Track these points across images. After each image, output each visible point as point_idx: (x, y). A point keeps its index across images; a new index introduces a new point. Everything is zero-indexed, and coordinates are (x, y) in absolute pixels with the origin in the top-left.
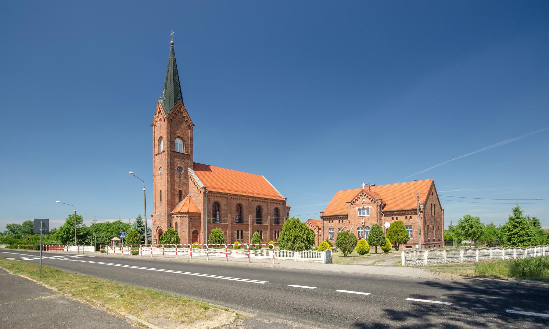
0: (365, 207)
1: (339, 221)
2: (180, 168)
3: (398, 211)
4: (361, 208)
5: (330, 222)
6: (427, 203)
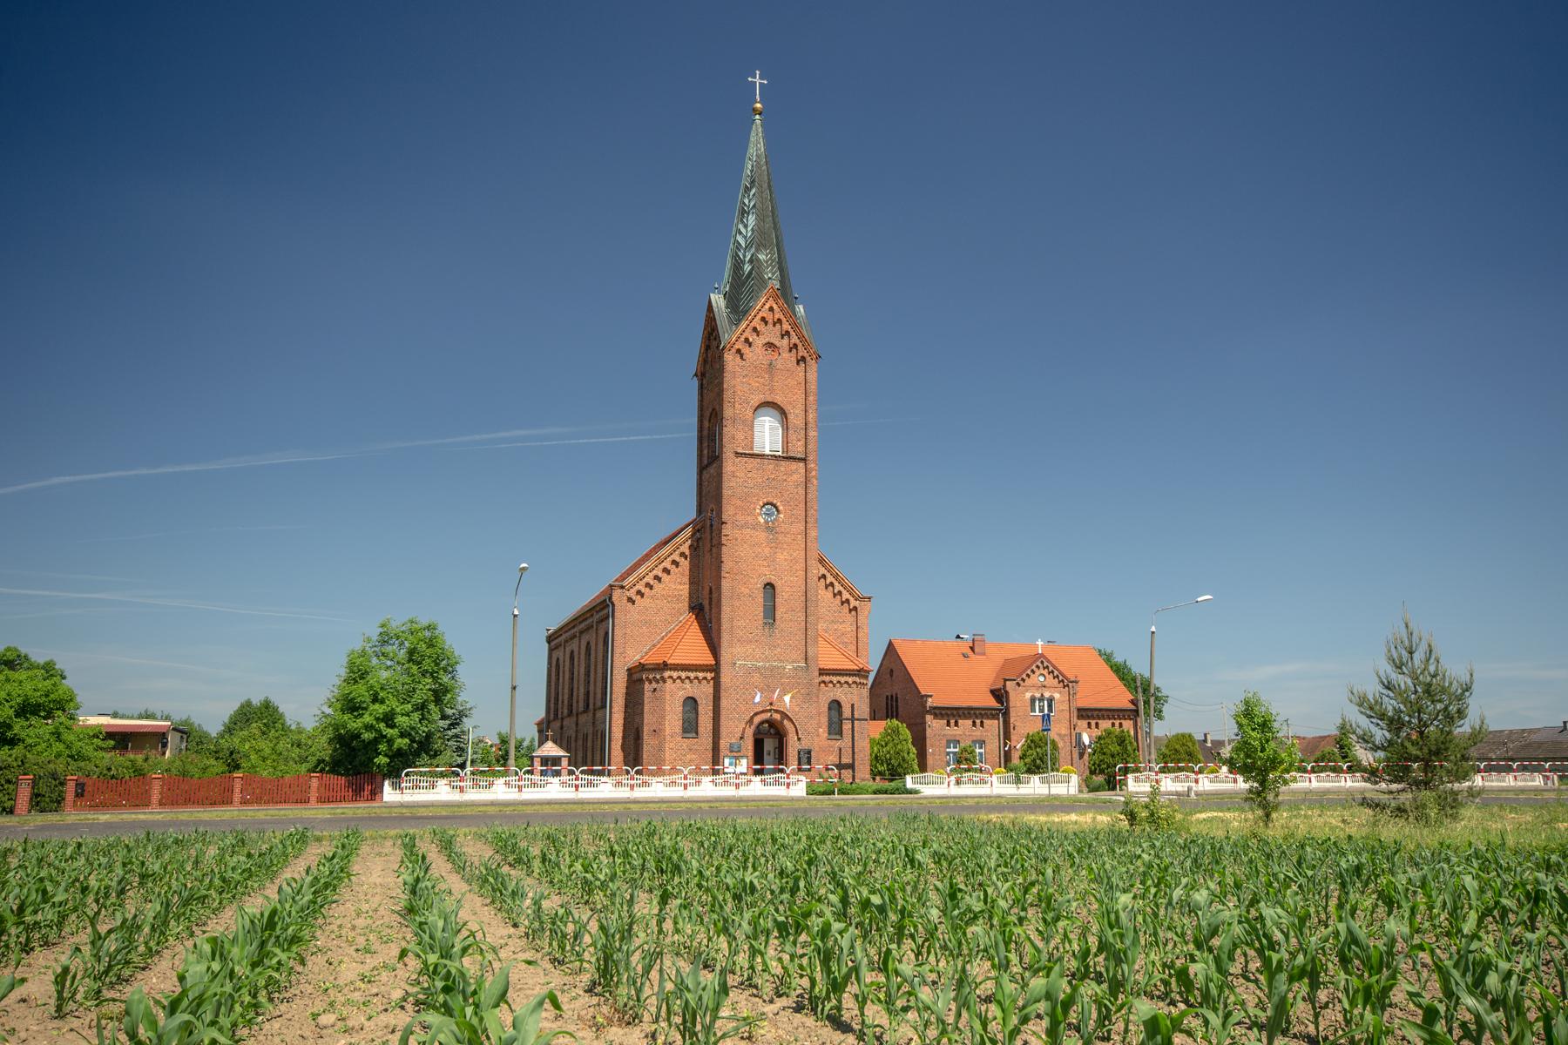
0: (1047, 695)
1: (974, 722)
2: (769, 507)
3: (1100, 710)
4: (1038, 695)
5: (974, 724)
6: (724, 548)
